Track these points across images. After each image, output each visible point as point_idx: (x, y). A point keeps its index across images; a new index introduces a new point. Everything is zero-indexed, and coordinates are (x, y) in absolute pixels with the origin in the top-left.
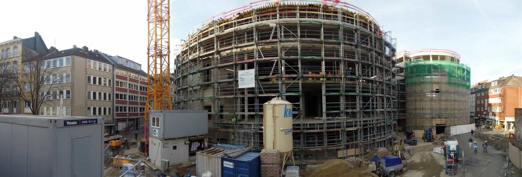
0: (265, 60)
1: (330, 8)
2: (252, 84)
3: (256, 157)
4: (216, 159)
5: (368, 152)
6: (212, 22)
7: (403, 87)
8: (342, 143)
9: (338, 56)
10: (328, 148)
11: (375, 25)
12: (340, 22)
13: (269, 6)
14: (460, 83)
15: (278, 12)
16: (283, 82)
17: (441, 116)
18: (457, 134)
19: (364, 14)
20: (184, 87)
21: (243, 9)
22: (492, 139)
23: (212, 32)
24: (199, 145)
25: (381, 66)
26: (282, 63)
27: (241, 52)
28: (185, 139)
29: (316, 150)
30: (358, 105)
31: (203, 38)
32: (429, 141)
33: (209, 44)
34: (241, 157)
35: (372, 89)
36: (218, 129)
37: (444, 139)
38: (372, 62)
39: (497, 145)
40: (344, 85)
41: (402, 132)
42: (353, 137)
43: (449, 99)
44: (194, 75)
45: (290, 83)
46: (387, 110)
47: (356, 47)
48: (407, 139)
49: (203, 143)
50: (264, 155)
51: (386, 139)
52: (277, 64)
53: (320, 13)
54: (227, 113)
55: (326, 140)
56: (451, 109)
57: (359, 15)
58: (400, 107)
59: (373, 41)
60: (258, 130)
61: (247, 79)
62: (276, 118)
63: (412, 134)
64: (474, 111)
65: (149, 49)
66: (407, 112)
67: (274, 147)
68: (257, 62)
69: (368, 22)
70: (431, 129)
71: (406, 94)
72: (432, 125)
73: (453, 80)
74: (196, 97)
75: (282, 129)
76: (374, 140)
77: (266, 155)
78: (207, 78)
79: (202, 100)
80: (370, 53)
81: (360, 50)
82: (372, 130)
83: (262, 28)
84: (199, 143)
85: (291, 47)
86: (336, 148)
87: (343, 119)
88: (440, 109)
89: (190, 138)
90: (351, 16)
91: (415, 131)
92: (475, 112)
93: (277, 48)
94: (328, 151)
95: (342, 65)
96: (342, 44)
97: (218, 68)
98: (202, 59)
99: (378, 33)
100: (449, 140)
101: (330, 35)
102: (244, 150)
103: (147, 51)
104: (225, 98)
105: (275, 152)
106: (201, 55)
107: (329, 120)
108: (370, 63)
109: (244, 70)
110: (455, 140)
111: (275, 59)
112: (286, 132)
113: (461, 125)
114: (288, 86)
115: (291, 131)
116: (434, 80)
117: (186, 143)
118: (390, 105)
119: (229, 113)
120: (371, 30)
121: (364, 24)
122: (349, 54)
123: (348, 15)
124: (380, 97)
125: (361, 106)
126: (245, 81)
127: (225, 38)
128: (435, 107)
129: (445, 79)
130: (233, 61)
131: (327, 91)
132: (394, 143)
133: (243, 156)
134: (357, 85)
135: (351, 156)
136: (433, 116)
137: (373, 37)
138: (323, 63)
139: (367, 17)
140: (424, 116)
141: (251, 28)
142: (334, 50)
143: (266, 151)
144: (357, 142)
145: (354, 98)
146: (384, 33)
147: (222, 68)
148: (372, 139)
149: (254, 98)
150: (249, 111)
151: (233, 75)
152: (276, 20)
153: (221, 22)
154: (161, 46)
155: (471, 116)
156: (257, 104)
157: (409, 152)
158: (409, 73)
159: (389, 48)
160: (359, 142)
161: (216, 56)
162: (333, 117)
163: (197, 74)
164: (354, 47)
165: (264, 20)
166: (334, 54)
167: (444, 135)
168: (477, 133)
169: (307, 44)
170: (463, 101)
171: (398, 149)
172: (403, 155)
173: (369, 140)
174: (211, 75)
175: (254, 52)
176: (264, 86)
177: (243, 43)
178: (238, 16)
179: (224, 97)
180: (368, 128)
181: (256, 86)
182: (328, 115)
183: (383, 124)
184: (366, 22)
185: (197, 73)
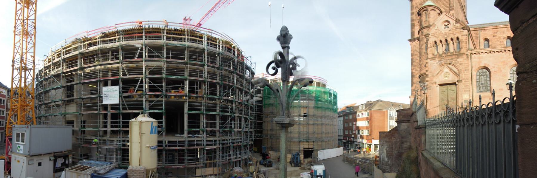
2: (115, 100)
4: (85, 176)
7: (260, 107)
8: (201, 161)
10: (189, 166)
11: (238, 49)
12: (204, 46)
14: (327, 107)
15: (144, 34)
16: (147, 99)
17: (309, 140)
18: (325, 158)
20: (45, 102)
21: (108, 29)
22: (359, 163)
23: (76, 49)
24: (64, 161)
25: (241, 87)
26: (146, 80)
28: (50, 155)
29: (177, 168)
30: (218, 124)
31: (66, 54)
32: (297, 165)
33: (72, 60)
35: (232, 109)
36: (81, 145)
37: (312, 164)
39: (364, 168)
40: (205, 104)
41: (258, 152)
42: (212, 156)
43: (316, 123)
44: (57, 90)
45: (153, 101)
46: (245, 130)
48: (263, 160)
50: (131, 172)
51: (242, 159)
52: (142, 82)
53: (185, 37)
54: (91, 129)
56: (318, 133)
57: (222, 40)
58: (256, 127)
60: (121, 146)
63: (268, 156)
64: (342, 134)
65: (13, 62)
66: (263, 133)
67: (140, 164)
70: (299, 153)
71: (263, 115)
72: (300, 149)
73: (320, 104)
74: (59, 113)
75: (148, 145)
76: (229, 160)
77: (133, 172)
79: (65, 115)
83: (126, 48)
84: (63, 158)
87: (202, 137)
88: (308, 133)
89: (55, 154)
90: (214, 41)
91: (270, 152)
92: (343, 135)
93: (142, 67)
94: (189, 168)
96: (206, 66)
97: (81, 84)
98: (65, 74)
99: (240, 57)
100: (316, 165)
101: (194, 57)
102: (110, 166)
103: (11, 64)
104: (89, 114)
105: (142, 169)
106: (64, 71)
107: (189, 137)
108: (231, 84)
109: (108, 86)
110: (321, 165)
111: (140, 77)
113: (329, 149)
114: (152, 103)
116: (302, 105)
117: (51, 159)
118: (247, 125)
119: (93, 129)
120: (234, 54)
121: (228, 48)
122: (211, 75)
123: (211, 40)
124: (238, 116)
125: (221, 125)
128: (303, 131)
129: (312, 104)
130: (97, 78)
131: (189, 109)
132: (250, 163)
133: (111, 173)
134: (218, 104)
136: (301, 139)
137: (236, 60)
138: (187, 83)
139: (231, 43)
140: (291, 140)
141: (117, 47)
142: (197, 71)
143: (133, 168)
145: (213, 117)
146: (246, 58)
147: (85, 84)
148: (228, 158)
150: (112, 127)
151: (98, 92)
154: (26, 59)
155: (339, 140)
156: (120, 120)
157: (264, 173)
158: (267, 95)
160: (217, 161)
161: (79, 72)
163: (61, 89)
165: (128, 40)
166: (198, 75)
167: (312, 159)
168: (345, 157)
169: (172, 64)
170: (331, 125)
171: (254, 170)
172: (258, 177)
174: (74, 91)
176: (128, 103)
178: (104, 35)
179: (87, 112)
181: (120, 103)
182: (189, 132)
183: (239, 144)
184: (230, 48)
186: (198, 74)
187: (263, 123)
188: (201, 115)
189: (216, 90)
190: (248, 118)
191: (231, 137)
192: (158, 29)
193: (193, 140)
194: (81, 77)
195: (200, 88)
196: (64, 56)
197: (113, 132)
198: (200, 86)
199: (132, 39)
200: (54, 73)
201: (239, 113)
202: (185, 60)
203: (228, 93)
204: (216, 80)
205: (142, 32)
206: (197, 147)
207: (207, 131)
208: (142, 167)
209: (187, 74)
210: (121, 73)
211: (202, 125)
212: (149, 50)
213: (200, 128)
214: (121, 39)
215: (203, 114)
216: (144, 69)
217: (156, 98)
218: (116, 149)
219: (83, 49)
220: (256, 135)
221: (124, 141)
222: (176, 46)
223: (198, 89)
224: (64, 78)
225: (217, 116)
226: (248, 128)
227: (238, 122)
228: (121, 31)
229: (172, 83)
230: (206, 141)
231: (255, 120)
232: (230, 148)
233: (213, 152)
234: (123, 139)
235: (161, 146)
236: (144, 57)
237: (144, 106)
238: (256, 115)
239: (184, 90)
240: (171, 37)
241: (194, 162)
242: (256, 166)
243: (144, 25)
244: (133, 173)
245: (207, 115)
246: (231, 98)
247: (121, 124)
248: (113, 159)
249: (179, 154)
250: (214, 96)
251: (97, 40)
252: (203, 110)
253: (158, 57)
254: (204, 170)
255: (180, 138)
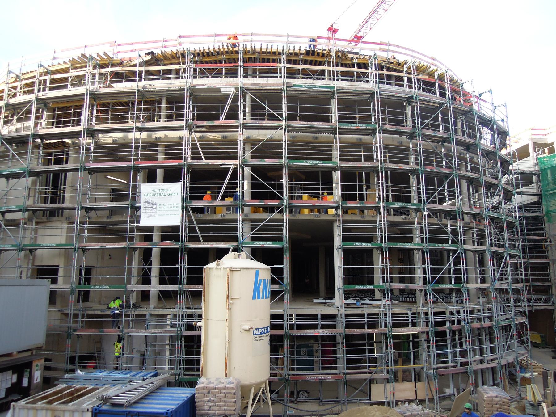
0: (208, 165)
1: (350, 55)
3: (186, 399)
5: (448, 394)
6: (80, 56)
8: (382, 366)
9: (369, 159)
10: (349, 377)
11: (452, 80)
12: (371, 86)
13: (221, 48)
16: (246, 216)
19: (425, 62)
21: (160, 44)
23: (79, 80)
26: (245, 172)
27: (151, 140)
30: (419, 273)
31: (51, 89)
34: (147, 401)
35: (454, 233)
38: (451, 168)
41: (543, 348)
44: (12, 181)
45: (262, 220)
46: (498, 285)
47: (412, 136)
49: (27, 374)
51: (499, 363)
54: (105, 288)
55: (341, 355)
57: (416, 64)
59: (451, 119)
60: (183, 328)
61: (162, 206)
62: (234, 301)
68: (190, 166)
69: (436, 77)
74: (15, 243)
75: (247, 327)
76: (464, 364)
77: (209, 393)
78: (53, 193)
79: (31, 251)
80: (445, 147)
81: (421, 142)
82: (457, 337)
84: (13, 373)
85: (267, 141)
86: (368, 376)
90: (395, 70)
94: (347, 383)
95: (379, 180)
96: (380, 133)
104: (103, 249)
105: (231, 386)
106: (41, 132)
107: (348, 306)
108: (446, 171)
109: (155, 182)
111: (231, 164)
112: (256, 333)
115: (267, 332)
120: (443, 95)
121: (425, 83)
123: (388, 69)
125: (429, 276)
126: (158, 209)
127: (113, 101)
130: (130, 160)
131: (345, 239)
133: (153, 399)
134: (416, 224)
135: (406, 401)
137: (450, 109)
138: (337, 176)
139: (432, 68)
141: (180, 90)
142: (360, 147)
143: (210, 383)
144: (421, 366)
147: (98, 174)
148: (460, 360)
149: (176, 251)
150: (162, 282)
151: (129, 194)
152: (235, 79)
153: (104, 62)
156: (183, 265)
159: (492, 129)
160: (424, 365)
161: (84, 141)
162: (358, 301)
164: (405, 137)
165: (208, 77)
166: (361, 156)
169: (302, 134)
171: (539, 398)
173: (450, 364)
174: (64, 188)
175: (182, 145)
177: (157, 121)
178: (149, 57)
180: (448, 332)
181: (182, 224)
182: (348, 295)
184: (431, 80)
185: (24, 177)
186: (362, 153)
187: (551, 263)
188: (375, 251)
189: (409, 188)
190: (503, 253)
191: (462, 307)
192: (274, 53)
193: (360, 312)
194: (86, 153)
195: (368, 187)
196: (44, 93)
197: (165, 296)
198: (368, 181)
199: (213, 74)
200: (10, 132)
201: (476, 243)
202: (331, 122)
203: (439, 194)
204: (407, 163)
205: (238, 59)
206: (370, 331)
207: (392, 291)
208: (231, 382)
209: (336, 154)
210: (187, 152)
211: (378, 276)
212: (252, 100)
213: (376, 284)
214: (192, 73)
215: (381, 249)
216: (240, 145)
217: (268, 214)
218: (171, 337)
219: (97, 83)
220: (531, 299)
221: (190, 316)
222: (310, 90)
223: (365, 188)
224: (39, 149)
225: (415, 252)
226: (506, 279)
227: (475, 265)
228: (193, 54)
229: (304, 177)
230: (392, 314)
231: (524, 258)
232: (463, 334)
233: (411, 344)
234: (189, 312)
235: (281, 327)
236: (241, 116)
237: (239, 234)
238: (527, 243)
239: (332, 193)
240: (299, 70)
241: (365, 368)
242: (546, 385)
243: (243, 43)
244: (209, 395)
245: (390, 250)
246: (450, 205)
247: (184, 275)
248: (162, 361)
249: (323, 346)
250: (405, 204)
251: (137, 69)
252: (379, 239)
253: (272, 117)
254: (392, 389)
255: (325, 308)
